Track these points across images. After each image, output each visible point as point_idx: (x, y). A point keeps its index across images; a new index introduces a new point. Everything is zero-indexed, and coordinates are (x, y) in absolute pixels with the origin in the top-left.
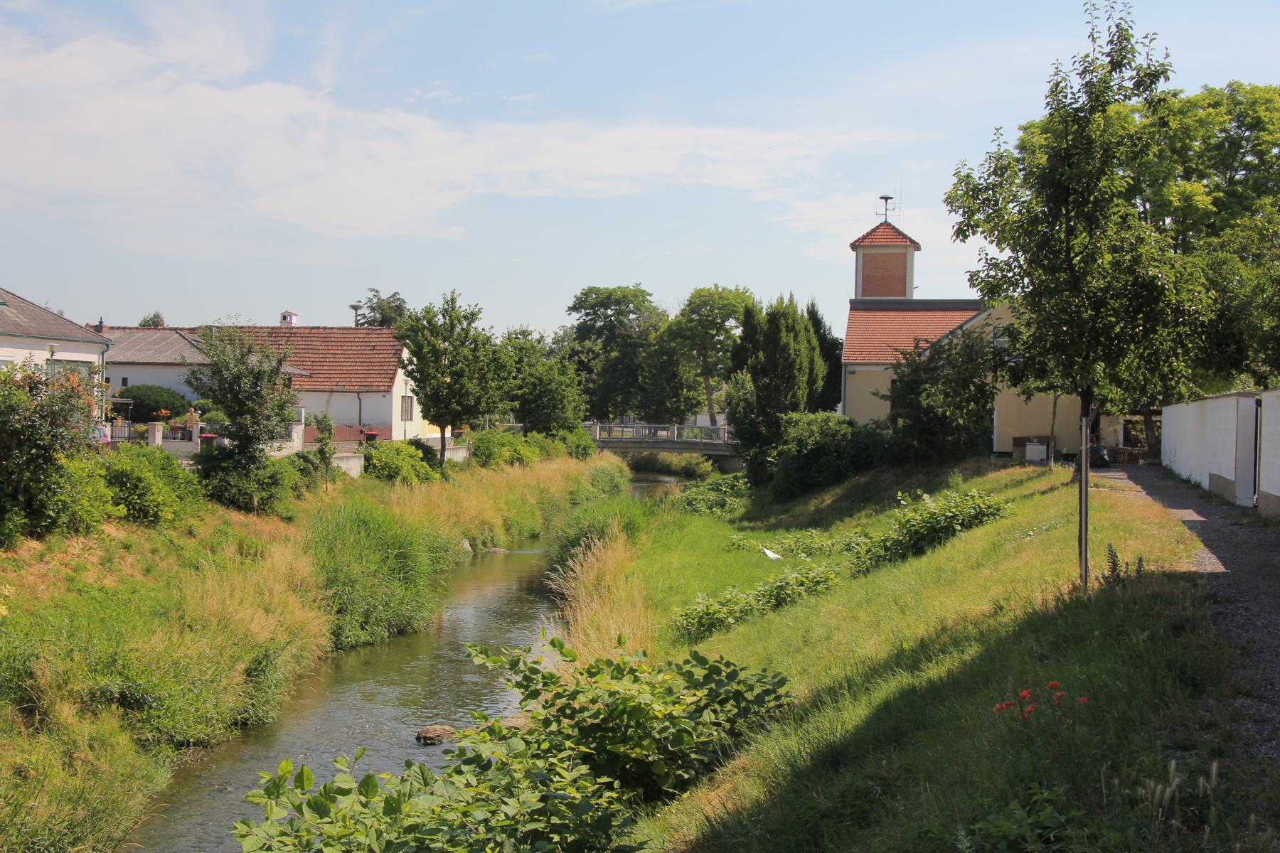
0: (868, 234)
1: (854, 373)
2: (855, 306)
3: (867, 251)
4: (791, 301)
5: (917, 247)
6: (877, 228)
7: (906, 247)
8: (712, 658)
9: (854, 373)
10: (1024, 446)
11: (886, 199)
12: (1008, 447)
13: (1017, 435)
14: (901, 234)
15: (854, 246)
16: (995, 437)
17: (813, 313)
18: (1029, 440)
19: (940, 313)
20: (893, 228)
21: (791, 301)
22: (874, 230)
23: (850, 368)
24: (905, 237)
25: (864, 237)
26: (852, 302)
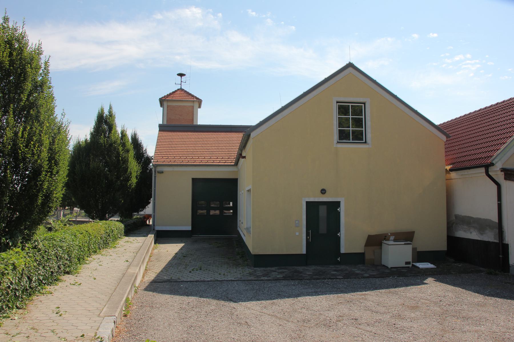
0: (170, 94)
1: (162, 172)
2: (162, 128)
3: (170, 104)
4: (110, 112)
5: (199, 102)
6: (176, 91)
7: (194, 101)
8: (144, 242)
9: (162, 172)
10: (380, 244)
11: (181, 75)
12: (358, 247)
13: (373, 232)
14: (190, 94)
15: (162, 101)
16: (343, 234)
17: (135, 140)
18: (385, 237)
19: (223, 134)
20: (186, 91)
21: (110, 112)
22: (174, 92)
23: (159, 169)
24: (193, 96)
25: (168, 96)
26: (160, 126)
